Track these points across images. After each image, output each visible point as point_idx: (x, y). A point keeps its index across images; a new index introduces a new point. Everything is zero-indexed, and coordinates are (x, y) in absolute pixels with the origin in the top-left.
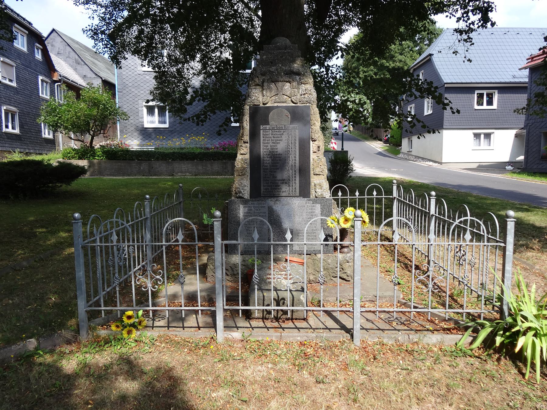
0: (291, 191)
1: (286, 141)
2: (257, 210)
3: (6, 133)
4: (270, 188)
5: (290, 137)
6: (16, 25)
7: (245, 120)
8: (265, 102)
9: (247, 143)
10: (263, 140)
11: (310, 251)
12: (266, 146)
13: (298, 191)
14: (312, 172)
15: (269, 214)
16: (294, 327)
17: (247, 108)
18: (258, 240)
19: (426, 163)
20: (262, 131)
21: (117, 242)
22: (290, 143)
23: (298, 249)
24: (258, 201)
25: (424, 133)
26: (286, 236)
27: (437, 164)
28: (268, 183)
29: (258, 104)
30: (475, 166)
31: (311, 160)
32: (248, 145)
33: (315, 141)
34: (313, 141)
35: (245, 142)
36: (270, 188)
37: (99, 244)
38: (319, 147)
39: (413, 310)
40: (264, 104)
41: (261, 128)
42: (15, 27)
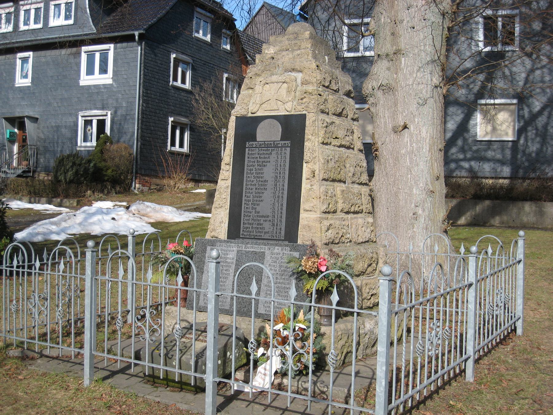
0: (275, 232)
1: (274, 163)
3: (172, 153)
5: (280, 157)
6: (199, 10)
8: (253, 112)
13: (283, 233)
15: (237, 260)
17: (233, 119)
18: (338, 304)
20: (247, 149)
21: (63, 272)
22: (279, 165)
26: (332, 297)
28: (249, 220)
37: (195, 289)
39: (105, 355)
40: (252, 113)
41: (247, 145)
42: (197, 12)
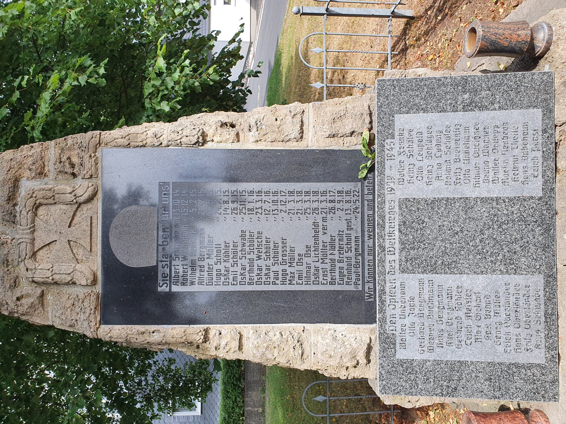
0: (347, 206)
2: (412, 307)
4: (338, 265)
7: (141, 339)
8: (91, 278)
9: (206, 331)
10: (200, 283)
11: (545, 144)
12: (219, 275)
14: (294, 146)
16: (37, 245)
19: (250, 62)
23: (539, 182)
24: (382, 302)
25: (211, 53)
27: (252, 49)
29: (93, 298)
30: (254, 12)
31: (261, 146)
32: (214, 329)
33: (204, 135)
34: (205, 142)
35: (206, 339)
36: (338, 265)
38: (223, 125)
